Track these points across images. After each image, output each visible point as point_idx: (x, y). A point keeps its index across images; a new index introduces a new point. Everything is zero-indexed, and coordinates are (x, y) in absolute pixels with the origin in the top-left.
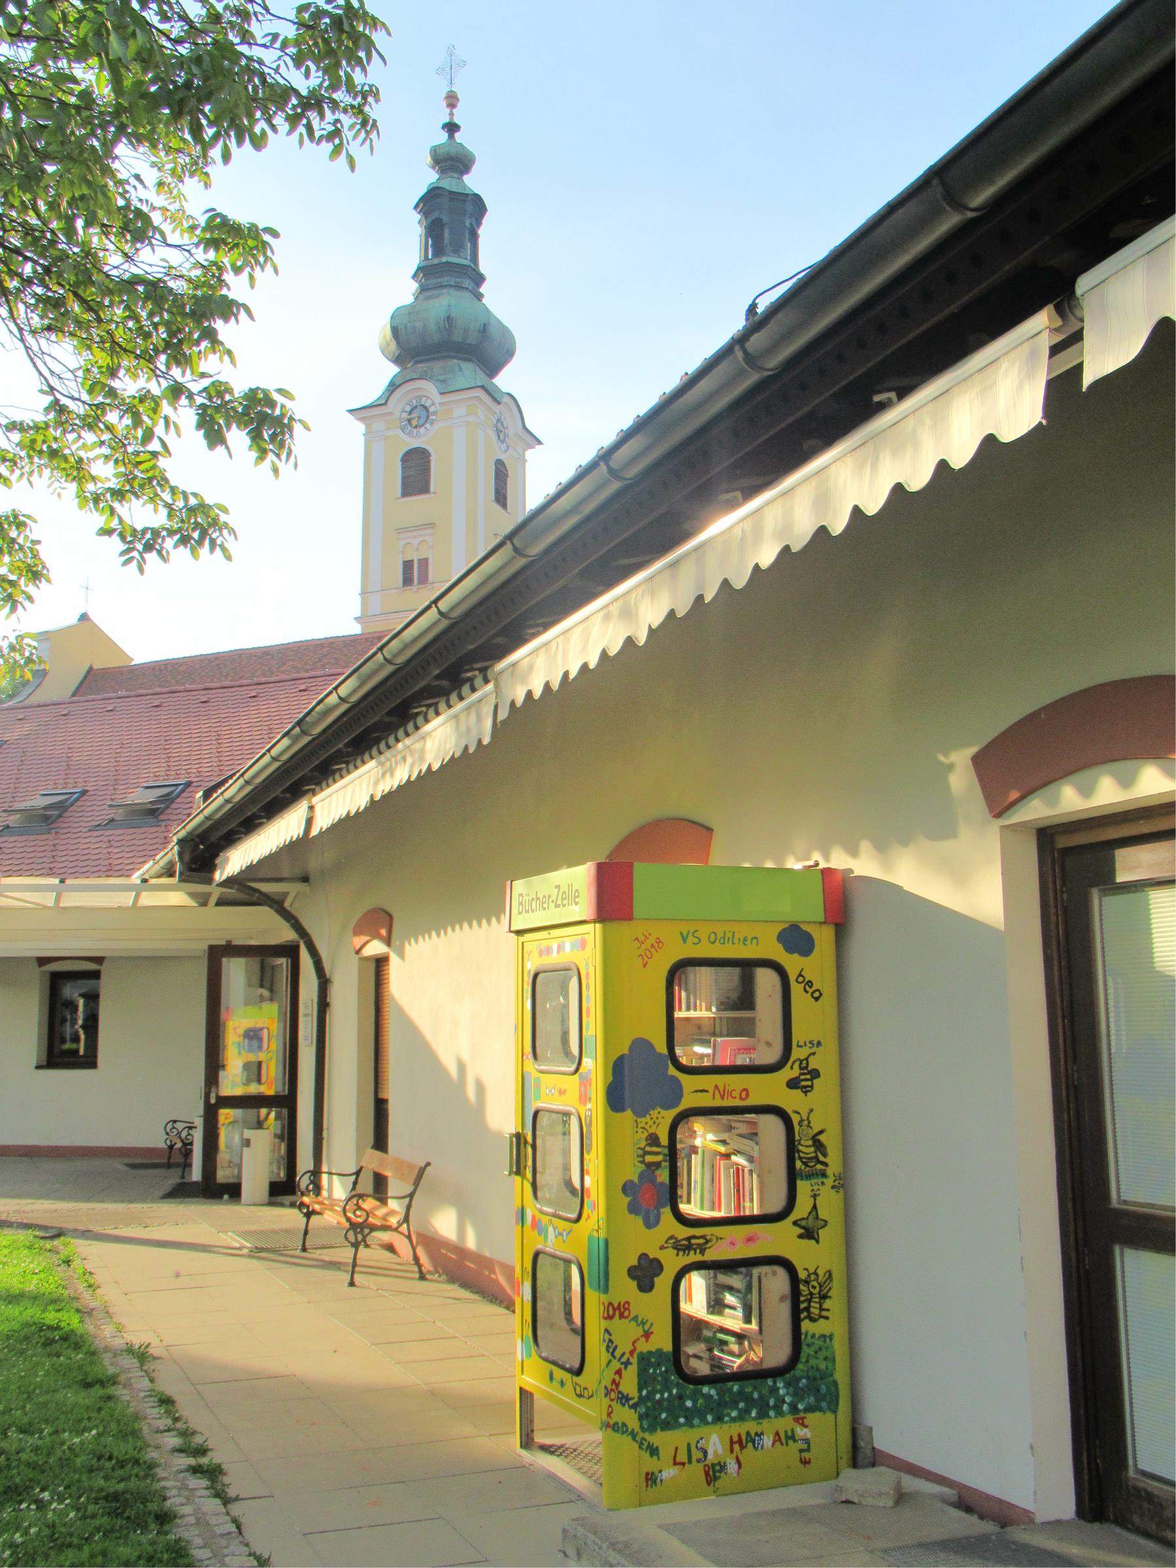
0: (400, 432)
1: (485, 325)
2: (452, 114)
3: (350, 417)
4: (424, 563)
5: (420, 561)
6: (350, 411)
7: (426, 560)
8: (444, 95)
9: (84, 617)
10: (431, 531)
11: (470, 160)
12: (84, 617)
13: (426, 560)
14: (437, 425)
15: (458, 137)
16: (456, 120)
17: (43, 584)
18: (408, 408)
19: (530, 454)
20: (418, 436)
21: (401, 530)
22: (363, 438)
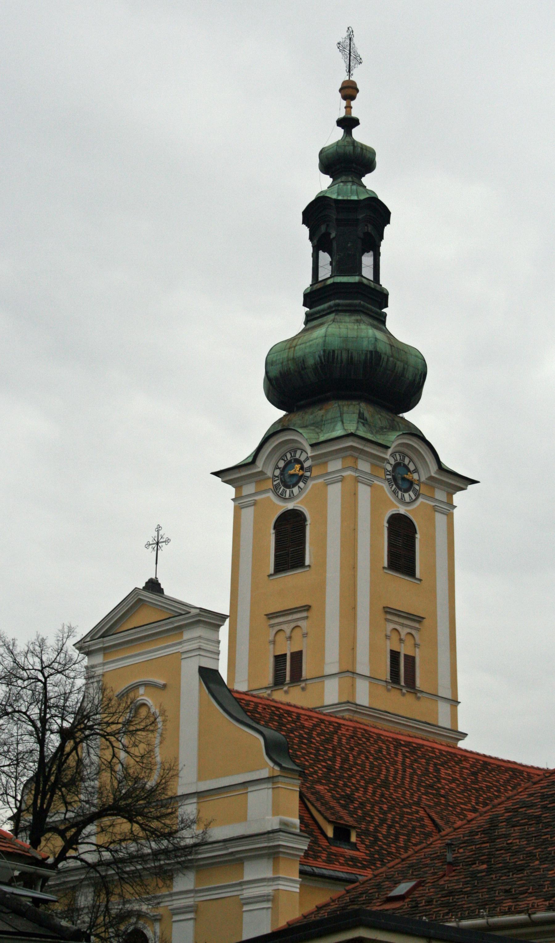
0: (271, 495)
1: (303, 361)
2: (348, 107)
3: (218, 480)
4: (297, 657)
5: (292, 654)
6: (217, 474)
7: (300, 653)
8: (339, 86)
9: (456, 507)
10: (304, 614)
11: (369, 155)
12: (456, 507)
13: (300, 653)
14: (311, 484)
15: (357, 134)
16: (354, 114)
17: (43, 635)
18: (282, 464)
19: (458, 498)
20: (292, 497)
21: (270, 616)
22: (232, 504)
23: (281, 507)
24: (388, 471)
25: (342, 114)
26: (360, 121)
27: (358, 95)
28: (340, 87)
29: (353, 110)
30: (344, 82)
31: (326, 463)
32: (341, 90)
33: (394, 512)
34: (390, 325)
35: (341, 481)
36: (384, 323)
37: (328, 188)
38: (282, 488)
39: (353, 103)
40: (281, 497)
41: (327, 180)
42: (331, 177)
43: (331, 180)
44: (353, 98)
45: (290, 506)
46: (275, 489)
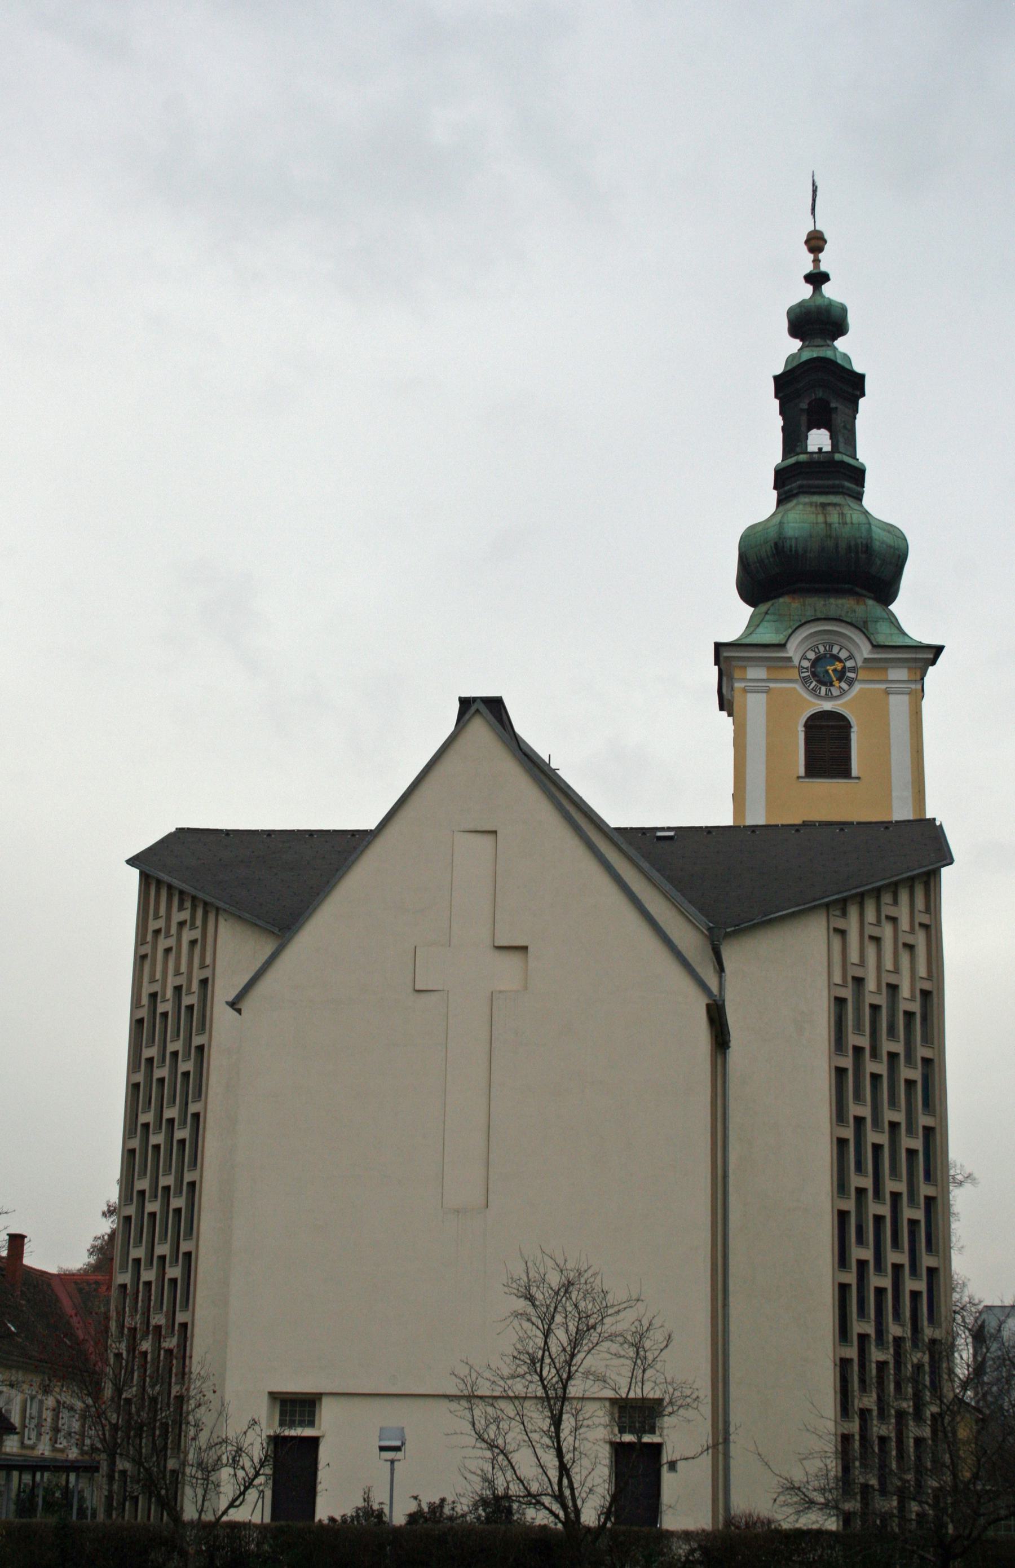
2: (816, 261)
15: (828, 290)
16: (823, 267)
23: (815, 704)
24: (804, 668)
25: (809, 268)
26: (831, 277)
27: (827, 247)
28: (805, 238)
29: (821, 264)
30: (810, 234)
31: (886, 669)
32: (807, 242)
33: (808, 716)
34: (864, 503)
35: (908, 694)
36: (861, 500)
37: (799, 350)
38: (814, 683)
39: (821, 256)
40: (814, 692)
41: (796, 344)
42: (801, 341)
43: (801, 343)
44: (820, 249)
45: (828, 706)
46: (805, 681)
